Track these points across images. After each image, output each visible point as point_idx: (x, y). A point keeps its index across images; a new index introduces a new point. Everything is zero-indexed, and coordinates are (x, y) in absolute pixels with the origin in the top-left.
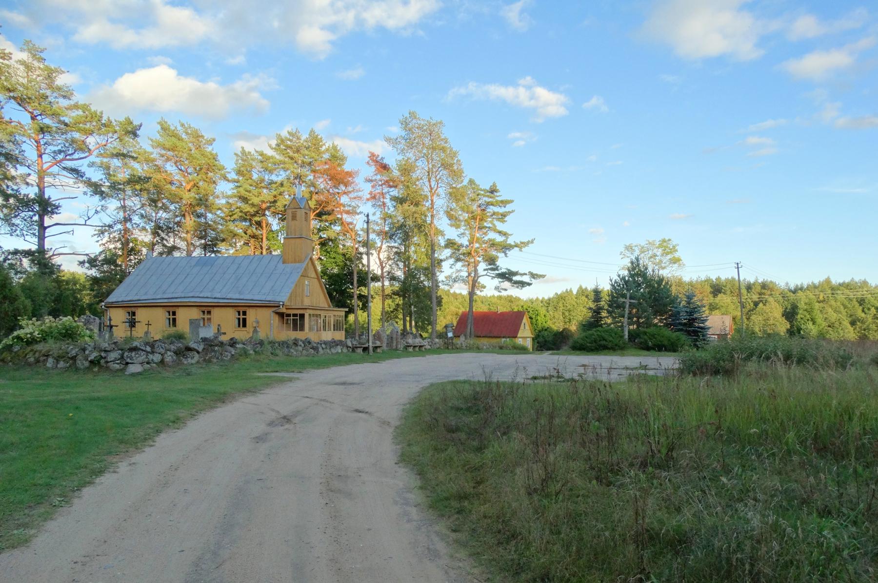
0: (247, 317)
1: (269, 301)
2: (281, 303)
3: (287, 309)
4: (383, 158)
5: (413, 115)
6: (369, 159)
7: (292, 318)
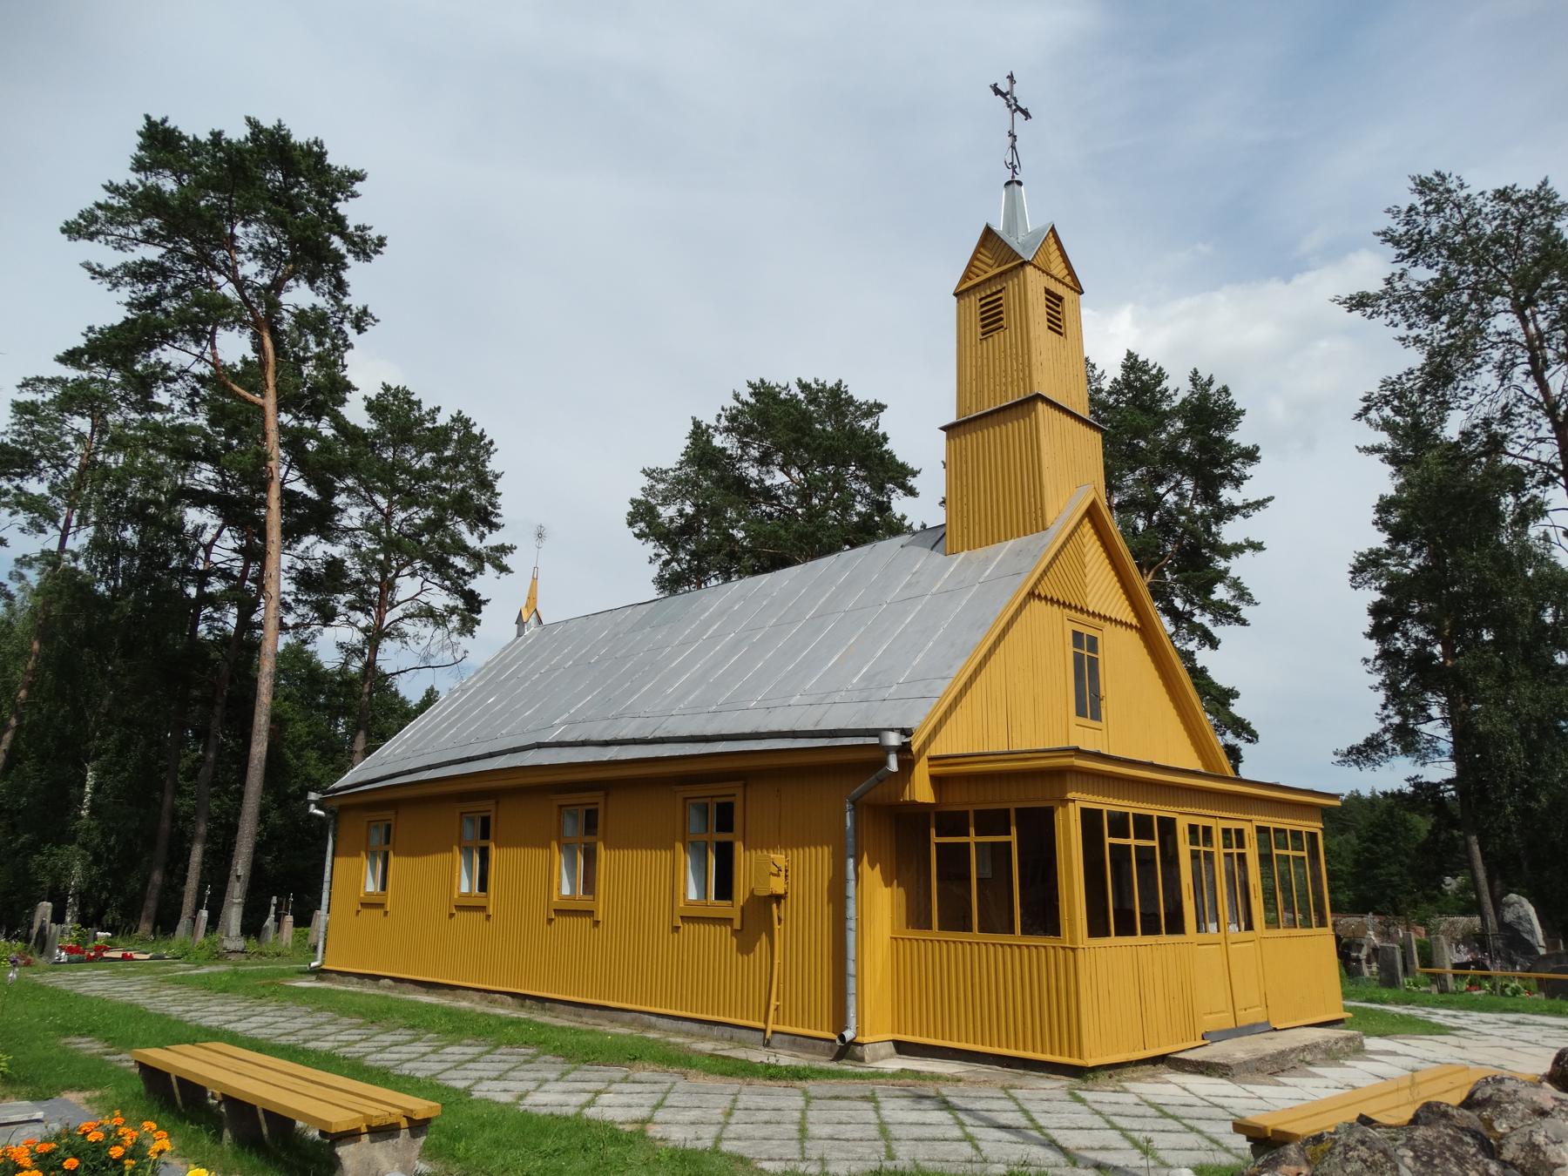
2: (894, 739)
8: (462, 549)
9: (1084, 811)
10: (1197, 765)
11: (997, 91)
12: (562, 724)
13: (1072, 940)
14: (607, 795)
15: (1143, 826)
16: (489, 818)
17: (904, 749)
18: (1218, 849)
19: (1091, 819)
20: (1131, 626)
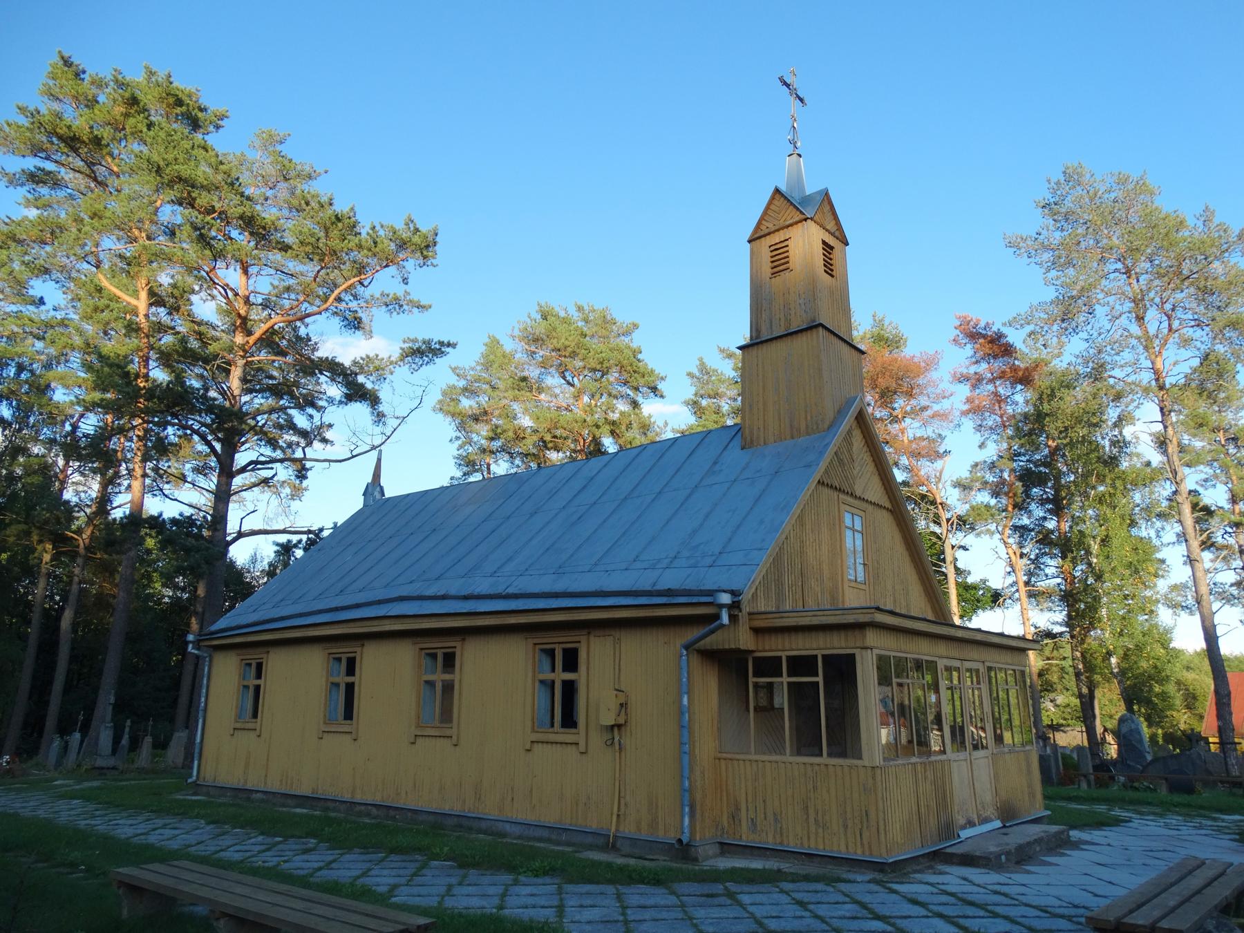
0: (580, 677)
1: (669, 593)
2: (725, 599)
3: (757, 631)
4: (987, 326)
5: (1072, 177)
6: (958, 332)
7: (785, 679)
8: (291, 426)
10: (930, 617)
16: (354, 659)
17: (735, 606)
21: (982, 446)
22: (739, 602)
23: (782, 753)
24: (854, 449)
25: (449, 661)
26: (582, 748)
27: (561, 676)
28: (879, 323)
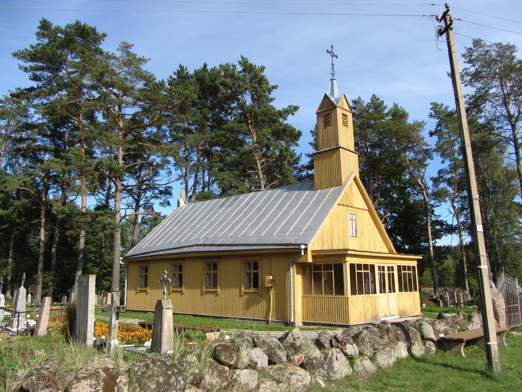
2: (303, 247)
5: (477, 43)
9: (350, 264)
11: (328, 52)
12: (203, 238)
13: (347, 295)
14: (220, 260)
15: (366, 267)
18: (386, 272)
19: (352, 266)
20: (448, 38)
21: (443, 162)
22: (307, 248)
23: (322, 294)
24: (353, 190)
25: (215, 267)
26: (260, 294)
27: (253, 271)
28: (396, 106)
